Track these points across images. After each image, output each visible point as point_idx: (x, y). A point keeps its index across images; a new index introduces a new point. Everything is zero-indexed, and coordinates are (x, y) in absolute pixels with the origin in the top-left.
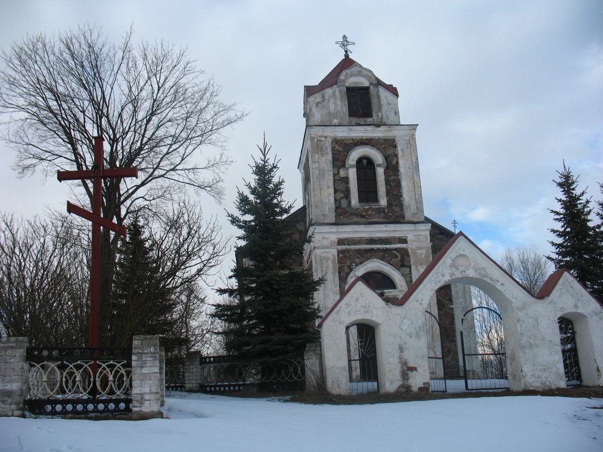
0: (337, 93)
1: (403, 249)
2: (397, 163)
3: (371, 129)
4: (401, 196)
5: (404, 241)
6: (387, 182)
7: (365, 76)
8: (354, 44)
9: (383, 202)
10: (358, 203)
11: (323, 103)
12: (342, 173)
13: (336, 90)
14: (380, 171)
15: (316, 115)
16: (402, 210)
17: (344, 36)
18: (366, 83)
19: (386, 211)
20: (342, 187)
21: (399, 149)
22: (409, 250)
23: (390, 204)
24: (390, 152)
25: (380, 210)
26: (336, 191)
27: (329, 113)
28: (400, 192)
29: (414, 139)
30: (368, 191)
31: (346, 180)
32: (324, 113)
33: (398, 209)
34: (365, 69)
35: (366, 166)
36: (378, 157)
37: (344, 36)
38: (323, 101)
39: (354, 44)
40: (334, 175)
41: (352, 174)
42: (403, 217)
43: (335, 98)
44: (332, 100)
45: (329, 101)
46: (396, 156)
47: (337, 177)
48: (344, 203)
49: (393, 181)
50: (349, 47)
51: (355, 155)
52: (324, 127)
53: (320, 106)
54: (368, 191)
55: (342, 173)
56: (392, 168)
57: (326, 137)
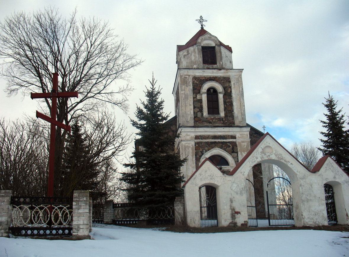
0: (196, 50)
1: (233, 142)
2: (231, 91)
3: (215, 71)
4: (233, 111)
5: (234, 137)
6: (225, 103)
7: (213, 40)
8: (206, 21)
9: (222, 114)
10: (207, 115)
11: (188, 56)
12: (198, 97)
13: (195, 48)
14: (221, 96)
15: (183, 63)
16: (233, 119)
17: (201, 17)
18: (213, 44)
19: (224, 119)
20: (198, 105)
21: (232, 83)
22: (237, 143)
23: (226, 116)
24: (227, 85)
25: (220, 119)
26: (194, 108)
27: (192, 61)
28: (232, 109)
29: (241, 78)
30: (213, 108)
31: (200, 101)
32: (188, 61)
33: (231, 119)
34: (213, 36)
35: (212, 93)
36: (219, 88)
37: (201, 17)
38: (188, 54)
39: (206, 21)
40: (194, 98)
41: (204, 97)
42: (234, 123)
43: (195, 53)
44: (193, 54)
45: (191, 55)
46: (230, 87)
47: (195, 99)
48: (199, 114)
49: (228, 102)
50: (204, 23)
51: (206, 86)
52: (188, 70)
53: (186, 57)
54: (213, 108)
55: (198, 97)
56: (228, 95)
57: (189, 76)
